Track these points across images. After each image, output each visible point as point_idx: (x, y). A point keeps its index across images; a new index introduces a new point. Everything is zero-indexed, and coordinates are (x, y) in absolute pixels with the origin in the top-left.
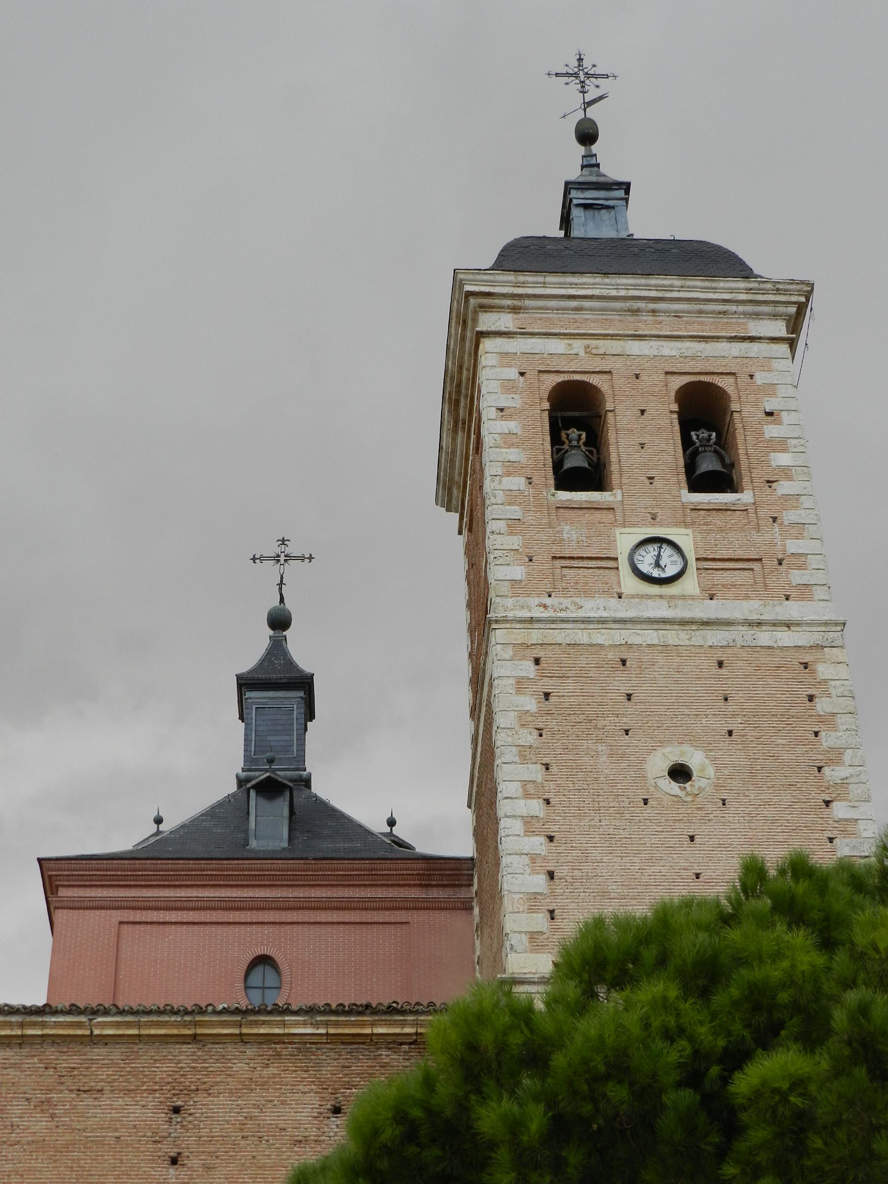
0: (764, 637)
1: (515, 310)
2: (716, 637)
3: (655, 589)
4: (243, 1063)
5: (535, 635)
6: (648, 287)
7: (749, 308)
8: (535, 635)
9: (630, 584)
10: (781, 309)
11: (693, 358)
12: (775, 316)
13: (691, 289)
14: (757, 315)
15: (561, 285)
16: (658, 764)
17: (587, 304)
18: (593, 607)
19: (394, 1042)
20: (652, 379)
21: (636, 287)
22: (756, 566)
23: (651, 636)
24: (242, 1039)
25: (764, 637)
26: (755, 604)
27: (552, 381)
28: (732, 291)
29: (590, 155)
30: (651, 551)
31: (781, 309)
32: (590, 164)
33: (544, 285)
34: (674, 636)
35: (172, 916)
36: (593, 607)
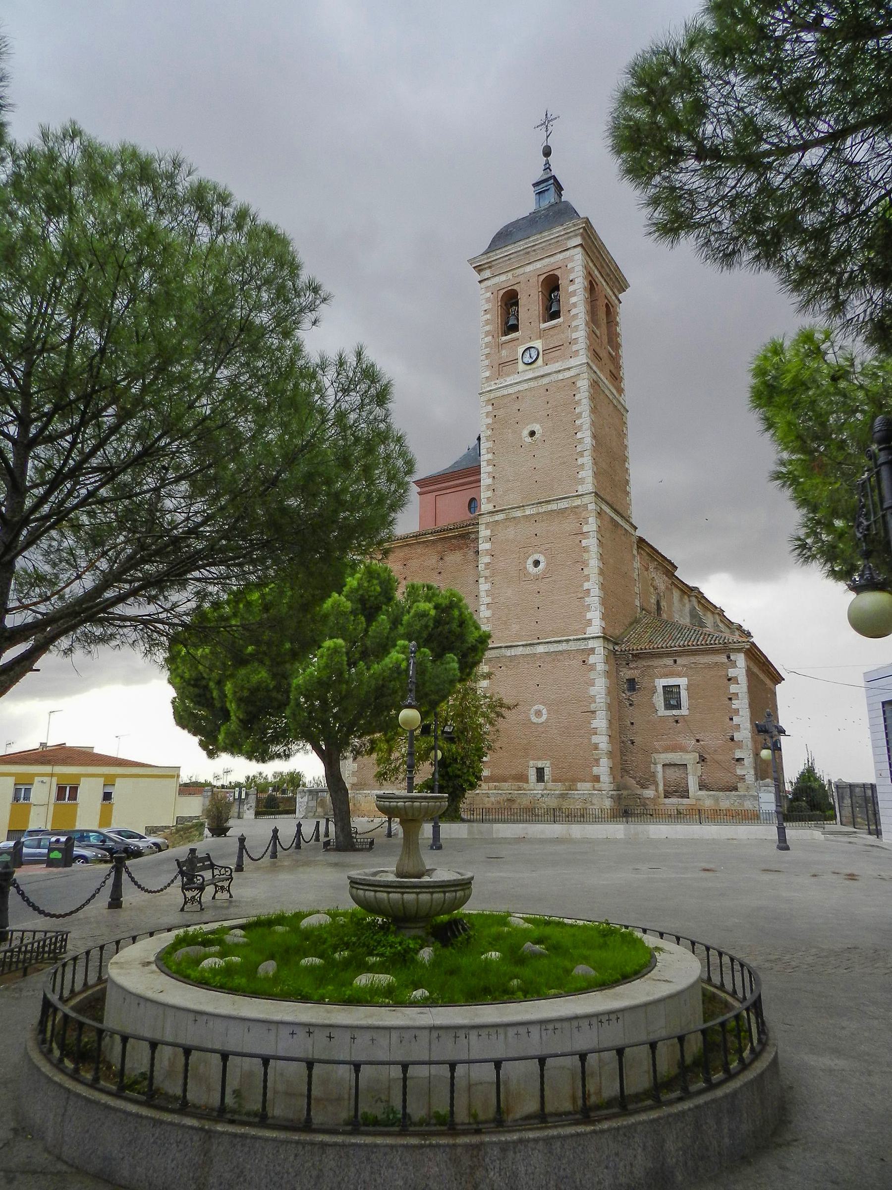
0: (561, 376)
1: (490, 267)
2: (545, 381)
3: (529, 367)
4: (419, 550)
5: (492, 395)
6: (530, 242)
7: (566, 236)
8: (492, 395)
9: (521, 367)
10: (577, 232)
11: (547, 265)
12: (576, 236)
13: (544, 237)
14: (569, 238)
15: (501, 253)
16: (526, 432)
17: (512, 256)
18: (510, 380)
19: (455, 537)
20: (534, 280)
21: (526, 244)
22: (561, 347)
23: (525, 386)
24: (419, 543)
25: (561, 376)
26: (560, 363)
27: (542, 278)
28: (558, 232)
29: (547, 163)
30: (527, 354)
31: (577, 232)
32: (547, 168)
33: (496, 255)
34: (532, 384)
35: (448, 491)
36: (516, 378)
